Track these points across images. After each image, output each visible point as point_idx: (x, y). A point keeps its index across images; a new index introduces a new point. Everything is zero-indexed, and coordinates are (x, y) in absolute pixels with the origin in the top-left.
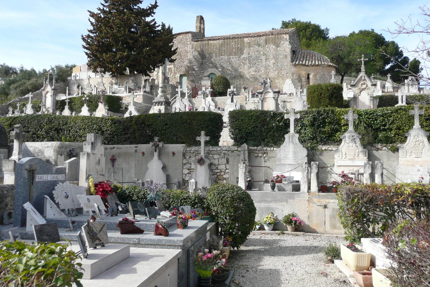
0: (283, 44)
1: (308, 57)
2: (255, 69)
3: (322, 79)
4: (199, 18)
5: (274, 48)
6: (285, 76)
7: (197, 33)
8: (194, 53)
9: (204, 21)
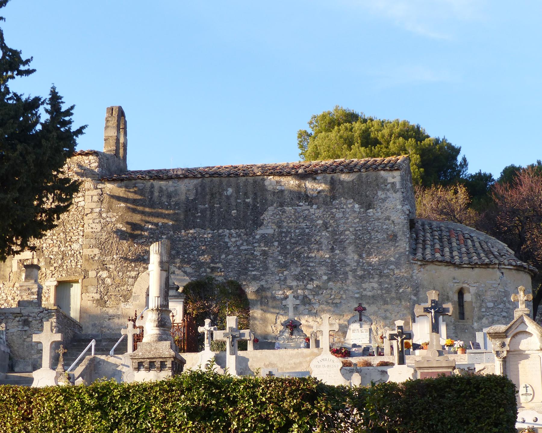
0: (384, 200)
1: (454, 240)
2: (299, 269)
3: (501, 306)
4: (115, 113)
5: (358, 210)
6: (393, 295)
7: (111, 156)
8: (104, 215)
9: (125, 122)
